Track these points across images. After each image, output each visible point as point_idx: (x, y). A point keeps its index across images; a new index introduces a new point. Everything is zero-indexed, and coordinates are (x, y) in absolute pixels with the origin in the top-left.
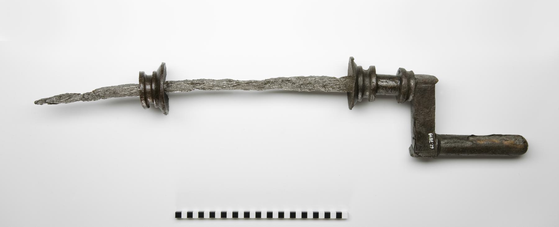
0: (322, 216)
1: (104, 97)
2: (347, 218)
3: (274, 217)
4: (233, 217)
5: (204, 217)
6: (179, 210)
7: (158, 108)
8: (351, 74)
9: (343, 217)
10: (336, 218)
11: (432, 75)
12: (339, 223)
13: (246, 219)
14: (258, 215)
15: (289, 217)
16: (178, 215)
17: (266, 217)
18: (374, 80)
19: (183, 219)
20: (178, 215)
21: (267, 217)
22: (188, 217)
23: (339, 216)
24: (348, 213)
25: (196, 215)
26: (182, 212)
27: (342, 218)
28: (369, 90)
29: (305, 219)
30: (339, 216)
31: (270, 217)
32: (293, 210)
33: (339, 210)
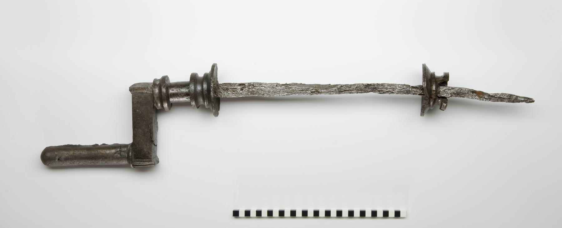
0: (380, 214)
1: (381, 92)
2: (405, 216)
3: (332, 215)
4: (291, 216)
5: (261, 216)
6: (236, 209)
7: (209, 108)
8: (436, 77)
9: (401, 215)
10: (383, 216)
11: (313, 84)
12: (397, 220)
13: (362, 218)
14: (328, 214)
15: (278, 215)
16: (236, 214)
17: (313, 216)
18: (164, 90)
19: (403, 218)
20: (236, 214)
21: (325, 216)
22: (245, 216)
23: (397, 214)
24: (406, 211)
25: (265, 214)
26: (239, 211)
27: (389, 216)
28: (212, 98)
29: (363, 218)
30: (397, 214)
31: (374, 216)
32: (351, 209)
33: (397, 209)
